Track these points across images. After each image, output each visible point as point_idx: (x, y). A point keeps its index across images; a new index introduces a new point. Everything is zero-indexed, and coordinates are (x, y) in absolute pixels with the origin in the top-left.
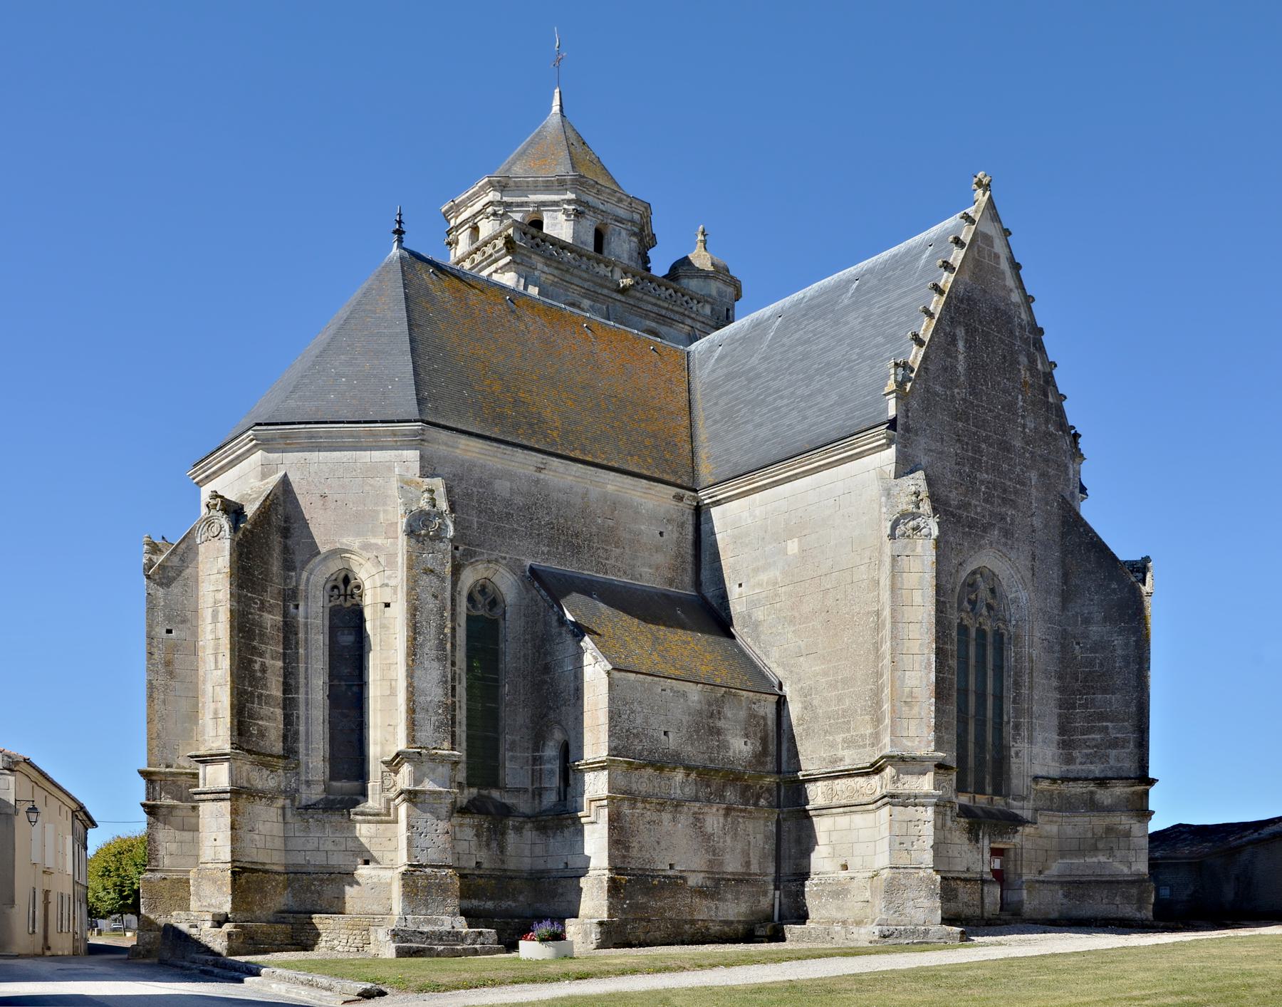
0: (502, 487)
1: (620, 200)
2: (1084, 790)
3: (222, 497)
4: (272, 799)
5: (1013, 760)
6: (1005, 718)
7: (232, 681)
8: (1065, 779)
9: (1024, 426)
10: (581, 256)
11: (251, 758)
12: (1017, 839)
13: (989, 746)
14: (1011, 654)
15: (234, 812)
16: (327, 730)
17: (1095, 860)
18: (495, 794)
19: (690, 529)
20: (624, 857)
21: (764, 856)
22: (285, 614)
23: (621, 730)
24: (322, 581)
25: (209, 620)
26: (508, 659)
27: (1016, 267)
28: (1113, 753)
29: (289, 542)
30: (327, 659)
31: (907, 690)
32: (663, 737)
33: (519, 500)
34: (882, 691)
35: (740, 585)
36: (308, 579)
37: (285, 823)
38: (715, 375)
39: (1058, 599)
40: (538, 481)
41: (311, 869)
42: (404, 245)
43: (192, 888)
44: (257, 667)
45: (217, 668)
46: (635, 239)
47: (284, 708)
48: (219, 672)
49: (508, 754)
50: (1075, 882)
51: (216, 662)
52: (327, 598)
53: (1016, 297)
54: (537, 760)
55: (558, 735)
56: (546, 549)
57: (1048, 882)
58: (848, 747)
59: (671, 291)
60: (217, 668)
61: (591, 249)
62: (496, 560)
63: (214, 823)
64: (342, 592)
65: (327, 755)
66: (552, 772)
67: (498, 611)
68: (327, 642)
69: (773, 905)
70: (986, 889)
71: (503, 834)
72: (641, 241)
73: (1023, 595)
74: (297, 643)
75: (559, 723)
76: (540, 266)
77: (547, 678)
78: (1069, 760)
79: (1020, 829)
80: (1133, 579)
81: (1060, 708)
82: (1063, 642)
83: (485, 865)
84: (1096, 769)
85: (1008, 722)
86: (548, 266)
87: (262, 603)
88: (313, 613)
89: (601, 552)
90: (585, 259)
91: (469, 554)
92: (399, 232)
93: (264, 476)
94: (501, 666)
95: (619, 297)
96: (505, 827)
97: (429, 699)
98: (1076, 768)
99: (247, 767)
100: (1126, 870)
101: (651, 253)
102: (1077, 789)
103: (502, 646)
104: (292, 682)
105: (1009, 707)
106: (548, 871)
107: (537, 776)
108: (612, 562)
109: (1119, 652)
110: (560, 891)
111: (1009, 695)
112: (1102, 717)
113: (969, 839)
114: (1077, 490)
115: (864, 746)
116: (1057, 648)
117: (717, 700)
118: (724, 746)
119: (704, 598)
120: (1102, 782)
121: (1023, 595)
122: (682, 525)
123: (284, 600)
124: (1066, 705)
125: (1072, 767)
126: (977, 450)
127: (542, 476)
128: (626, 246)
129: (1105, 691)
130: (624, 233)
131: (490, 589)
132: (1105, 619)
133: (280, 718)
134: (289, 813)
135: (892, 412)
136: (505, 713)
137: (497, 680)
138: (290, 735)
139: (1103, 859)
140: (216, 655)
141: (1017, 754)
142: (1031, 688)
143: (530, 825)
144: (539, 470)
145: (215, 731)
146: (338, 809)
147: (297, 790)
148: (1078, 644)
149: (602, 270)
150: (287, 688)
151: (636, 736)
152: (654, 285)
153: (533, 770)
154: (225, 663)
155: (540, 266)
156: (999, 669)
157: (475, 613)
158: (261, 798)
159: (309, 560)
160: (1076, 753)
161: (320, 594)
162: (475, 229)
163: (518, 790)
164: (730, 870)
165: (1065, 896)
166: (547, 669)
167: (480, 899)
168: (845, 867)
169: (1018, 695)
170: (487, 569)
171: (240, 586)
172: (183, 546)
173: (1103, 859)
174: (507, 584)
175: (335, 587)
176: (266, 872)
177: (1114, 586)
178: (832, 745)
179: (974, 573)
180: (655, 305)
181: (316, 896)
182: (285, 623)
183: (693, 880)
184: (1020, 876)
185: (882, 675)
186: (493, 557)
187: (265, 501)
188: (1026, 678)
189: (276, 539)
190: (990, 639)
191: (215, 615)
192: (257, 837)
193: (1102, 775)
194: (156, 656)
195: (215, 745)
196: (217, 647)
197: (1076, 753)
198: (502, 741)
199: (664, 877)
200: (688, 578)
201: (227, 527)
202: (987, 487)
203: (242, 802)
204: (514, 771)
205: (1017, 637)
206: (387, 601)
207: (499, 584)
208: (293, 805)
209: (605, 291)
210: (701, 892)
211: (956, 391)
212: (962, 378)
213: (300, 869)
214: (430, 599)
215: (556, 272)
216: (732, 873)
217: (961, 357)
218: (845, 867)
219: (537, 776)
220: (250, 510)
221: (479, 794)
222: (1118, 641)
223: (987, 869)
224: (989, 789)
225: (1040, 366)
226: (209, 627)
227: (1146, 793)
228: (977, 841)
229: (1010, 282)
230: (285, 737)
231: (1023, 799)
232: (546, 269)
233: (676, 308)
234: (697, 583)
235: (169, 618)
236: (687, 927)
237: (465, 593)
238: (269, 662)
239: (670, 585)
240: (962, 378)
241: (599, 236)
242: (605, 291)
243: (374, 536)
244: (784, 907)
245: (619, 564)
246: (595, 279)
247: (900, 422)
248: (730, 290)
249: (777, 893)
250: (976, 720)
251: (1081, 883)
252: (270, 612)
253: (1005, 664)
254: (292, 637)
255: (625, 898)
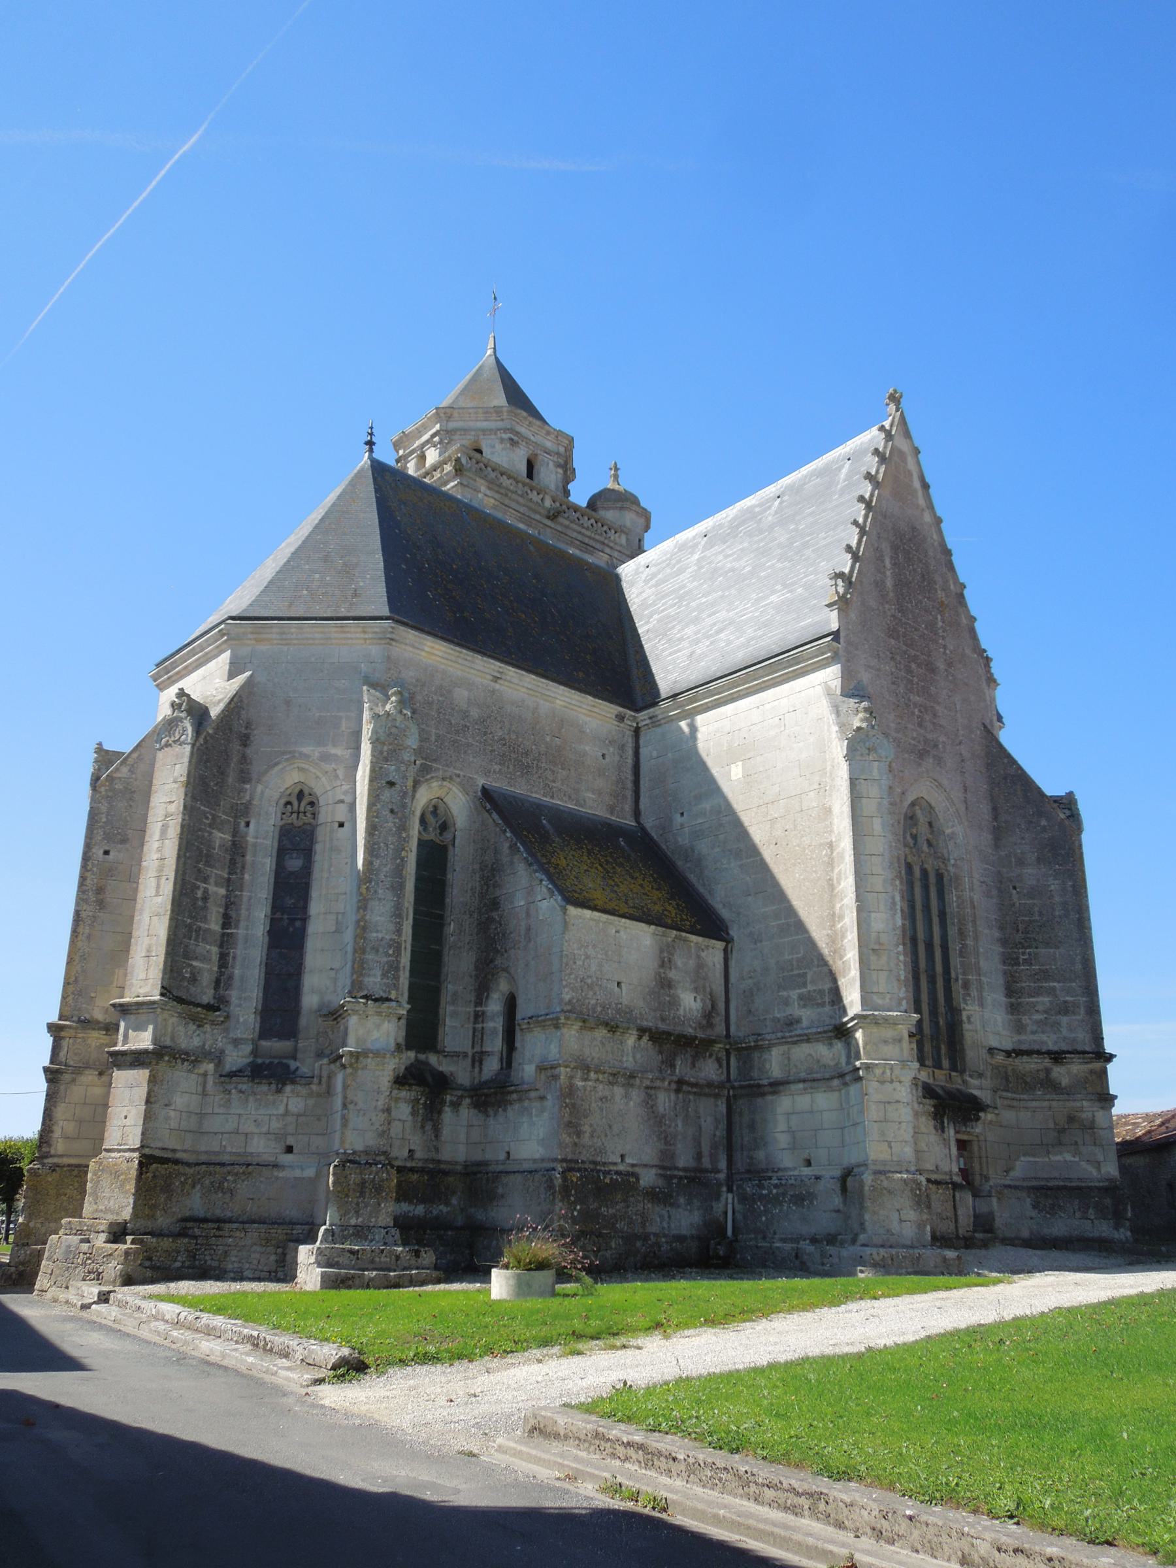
0: (461, 696)
1: (548, 433)
2: (1039, 1067)
3: (188, 696)
4: (196, 1062)
5: (966, 1026)
6: (953, 975)
7: (172, 911)
8: (1020, 1053)
9: (945, 647)
10: (517, 482)
11: (179, 1008)
12: (978, 1129)
13: (942, 1009)
14: (952, 898)
15: (152, 1080)
16: (263, 975)
17: (1059, 1158)
18: (433, 1059)
19: (630, 752)
20: (575, 1144)
21: (714, 1147)
22: (235, 832)
23: (576, 979)
24: (276, 796)
25: (157, 836)
26: (455, 891)
27: (926, 486)
28: (1065, 1020)
29: (248, 751)
30: (272, 887)
31: (874, 935)
32: (616, 989)
33: (475, 713)
34: (843, 937)
35: (682, 814)
36: (262, 793)
37: (204, 1094)
38: (644, 595)
39: (990, 837)
40: (493, 692)
41: (226, 1158)
42: (374, 455)
43: (89, 1185)
44: (199, 894)
45: (157, 894)
46: (560, 471)
47: (221, 946)
48: (160, 899)
49: (450, 1008)
50: (1042, 1188)
51: (158, 886)
52: (279, 815)
53: (927, 518)
54: (479, 1017)
55: (503, 986)
56: (497, 768)
57: (1016, 1187)
58: (805, 1006)
59: (593, 521)
60: (157, 894)
61: (525, 475)
62: (451, 778)
63: (128, 1095)
64: (296, 808)
65: (260, 1007)
66: (494, 1031)
67: (448, 836)
68: (274, 867)
69: (726, 1213)
70: (957, 1195)
71: (440, 1112)
72: (565, 472)
73: (959, 830)
74: (243, 867)
75: (506, 970)
76: (483, 489)
77: (495, 915)
78: (1019, 1028)
79: (982, 1114)
80: (1062, 816)
81: (1004, 963)
82: (1002, 886)
83: (419, 1155)
84: (1050, 1042)
85: (957, 980)
86: (489, 488)
87: (214, 817)
88: (262, 833)
89: (548, 773)
90: (520, 485)
91: (425, 770)
92: (370, 444)
93: (232, 675)
94: (448, 900)
95: (548, 522)
96: (443, 1102)
97: (380, 935)
98: (1029, 1040)
99: (174, 1020)
100: (1095, 1173)
101: (570, 487)
102: (1030, 1065)
103: (449, 876)
104: (233, 914)
105: (955, 961)
106: (485, 1163)
107: (478, 1036)
108: (558, 784)
109: (1057, 899)
110: (500, 1191)
111: (954, 947)
112: (1046, 975)
113: (935, 1128)
114: (995, 718)
115: (823, 1005)
116: (995, 892)
117: (668, 945)
118: (674, 1003)
119: (643, 829)
120: (1057, 1057)
121: (959, 830)
122: (622, 748)
123: (236, 817)
124: (1010, 960)
125: (1023, 1037)
126: (909, 671)
127: (497, 686)
128: (553, 477)
129: (1047, 945)
130: (551, 464)
131: (441, 811)
132: (1039, 860)
133: (215, 958)
134: (210, 1080)
135: (835, 626)
136: (449, 957)
137: (441, 917)
138: (222, 981)
139: (1068, 1157)
140: (158, 878)
141: (969, 1018)
142: (976, 939)
143: (468, 1101)
144: (496, 679)
145: (144, 977)
146: (266, 1077)
147: (222, 1052)
148: (1015, 888)
149: (534, 496)
150: (227, 921)
151: (590, 987)
152: (578, 514)
153: (474, 1030)
154: (168, 888)
155: (483, 489)
156: (942, 915)
157: (426, 837)
158: (184, 1060)
159: (266, 771)
160: (1025, 1019)
161: (272, 810)
162: (422, 458)
163: (457, 1055)
164: (681, 1163)
165: (1034, 1207)
166: (495, 904)
167: (411, 1202)
168: (809, 1163)
169: (964, 946)
170: (441, 787)
171: (194, 798)
172: (135, 755)
173: (1068, 1157)
174: (459, 805)
175: (289, 803)
176: (177, 1162)
177: (1044, 822)
178: (786, 1002)
179: (913, 804)
180: (580, 533)
181: (228, 1195)
182: (234, 843)
183: (648, 1178)
184: (987, 1179)
185: (841, 917)
186: (448, 774)
187: (230, 703)
188: (970, 927)
189: (236, 746)
190: (932, 879)
191: (164, 828)
192: (172, 1114)
193: (1055, 1048)
194: (88, 882)
195: (142, 991)
196: (160, 869)
197: (1025, 1019)
198: (444, 991)
199: (617, 1173)
200: (628, 807)
201: (190, 729)
202: (920, 711)
203: (162, 1066)
204: (454, 1031)
205: (957, 877)
206: (341, 820)
207: (451, 805)
208: (215, 1071)
209: (537, 517)
210: (653, 1195)
211: (887, 606)
212: (891, 594)
213: (214, 1159)
214: (390, 817)
215: (497, 496)
216: (685, 1169)
217: (888, 573)
218: (809, 1163)
219: (478, 1036)
220: (214, 712)
221: (417, 1060)
222: (1054, 885)
223: (955, 1169)
224: (946, 1063)
225: (952, 587)
226: (156, 845)
227: (1104, 1072)
228: (943, 1131)
229: (921, 502)
230: (217, 982)
231: (980, 1075)
232: (488, 493)
233: (597, 537)
234: (637, 813)
235: (108, 837)
236: (639, 1244)
237: (418, 814)
238: (212, 888)
239: (612, 813)
240: (891, 594)
241: (530, 466)
242: (537, 517)
243: (334, 746)
244: (739, 1216)
245: (564, 788)
246: (530, 504)
247: (842, 634)
248: (642, 521)
249: (730, 1196)
250: (928, 976)
251: (1050, 1188)
252: (219, 830)
253: (948, 910)
254: (239, 859)
255: (575, 1203)
